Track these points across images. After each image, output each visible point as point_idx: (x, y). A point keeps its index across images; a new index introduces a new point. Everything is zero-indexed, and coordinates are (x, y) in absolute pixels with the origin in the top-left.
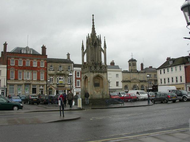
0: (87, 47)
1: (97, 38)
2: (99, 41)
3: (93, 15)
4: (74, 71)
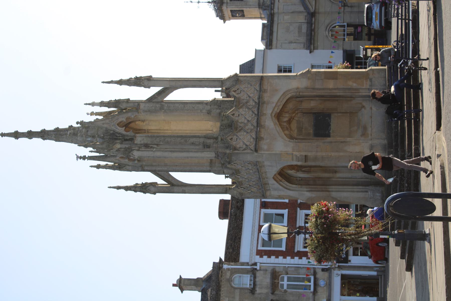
0: (142, 169)
1: (100, 117)
4: (257, 259)
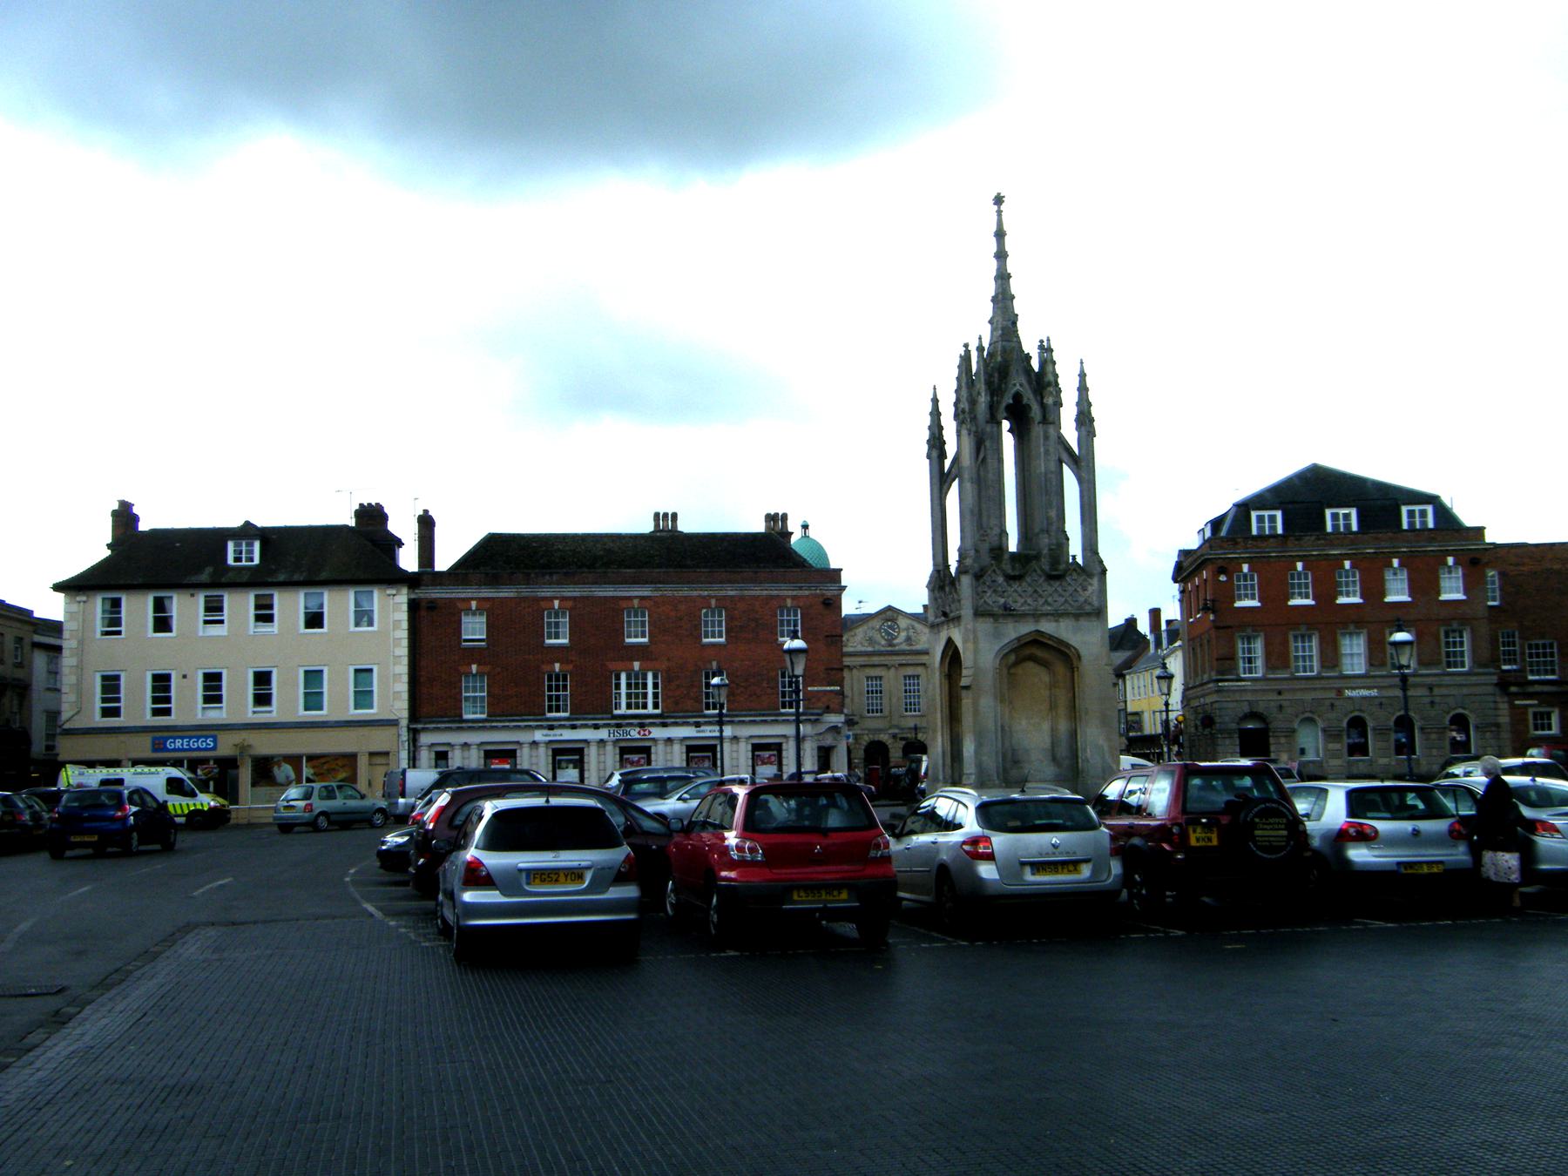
2: (1044, 382)
3: (999, 200)
